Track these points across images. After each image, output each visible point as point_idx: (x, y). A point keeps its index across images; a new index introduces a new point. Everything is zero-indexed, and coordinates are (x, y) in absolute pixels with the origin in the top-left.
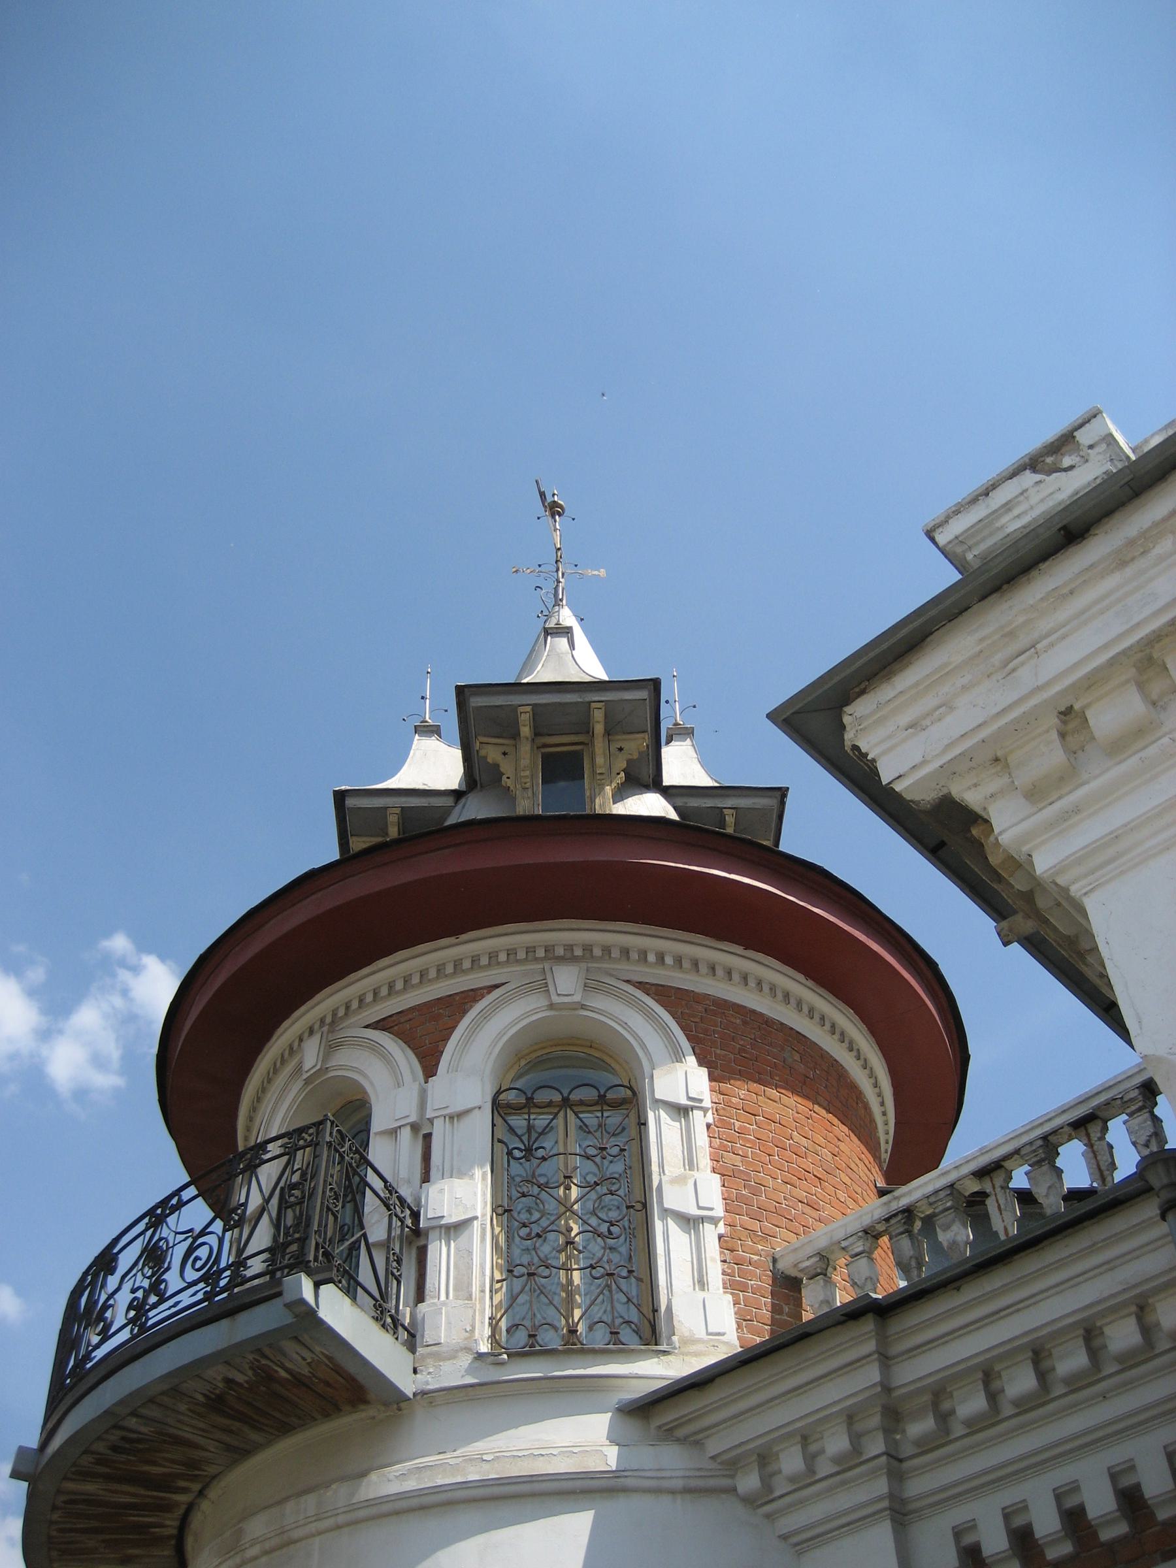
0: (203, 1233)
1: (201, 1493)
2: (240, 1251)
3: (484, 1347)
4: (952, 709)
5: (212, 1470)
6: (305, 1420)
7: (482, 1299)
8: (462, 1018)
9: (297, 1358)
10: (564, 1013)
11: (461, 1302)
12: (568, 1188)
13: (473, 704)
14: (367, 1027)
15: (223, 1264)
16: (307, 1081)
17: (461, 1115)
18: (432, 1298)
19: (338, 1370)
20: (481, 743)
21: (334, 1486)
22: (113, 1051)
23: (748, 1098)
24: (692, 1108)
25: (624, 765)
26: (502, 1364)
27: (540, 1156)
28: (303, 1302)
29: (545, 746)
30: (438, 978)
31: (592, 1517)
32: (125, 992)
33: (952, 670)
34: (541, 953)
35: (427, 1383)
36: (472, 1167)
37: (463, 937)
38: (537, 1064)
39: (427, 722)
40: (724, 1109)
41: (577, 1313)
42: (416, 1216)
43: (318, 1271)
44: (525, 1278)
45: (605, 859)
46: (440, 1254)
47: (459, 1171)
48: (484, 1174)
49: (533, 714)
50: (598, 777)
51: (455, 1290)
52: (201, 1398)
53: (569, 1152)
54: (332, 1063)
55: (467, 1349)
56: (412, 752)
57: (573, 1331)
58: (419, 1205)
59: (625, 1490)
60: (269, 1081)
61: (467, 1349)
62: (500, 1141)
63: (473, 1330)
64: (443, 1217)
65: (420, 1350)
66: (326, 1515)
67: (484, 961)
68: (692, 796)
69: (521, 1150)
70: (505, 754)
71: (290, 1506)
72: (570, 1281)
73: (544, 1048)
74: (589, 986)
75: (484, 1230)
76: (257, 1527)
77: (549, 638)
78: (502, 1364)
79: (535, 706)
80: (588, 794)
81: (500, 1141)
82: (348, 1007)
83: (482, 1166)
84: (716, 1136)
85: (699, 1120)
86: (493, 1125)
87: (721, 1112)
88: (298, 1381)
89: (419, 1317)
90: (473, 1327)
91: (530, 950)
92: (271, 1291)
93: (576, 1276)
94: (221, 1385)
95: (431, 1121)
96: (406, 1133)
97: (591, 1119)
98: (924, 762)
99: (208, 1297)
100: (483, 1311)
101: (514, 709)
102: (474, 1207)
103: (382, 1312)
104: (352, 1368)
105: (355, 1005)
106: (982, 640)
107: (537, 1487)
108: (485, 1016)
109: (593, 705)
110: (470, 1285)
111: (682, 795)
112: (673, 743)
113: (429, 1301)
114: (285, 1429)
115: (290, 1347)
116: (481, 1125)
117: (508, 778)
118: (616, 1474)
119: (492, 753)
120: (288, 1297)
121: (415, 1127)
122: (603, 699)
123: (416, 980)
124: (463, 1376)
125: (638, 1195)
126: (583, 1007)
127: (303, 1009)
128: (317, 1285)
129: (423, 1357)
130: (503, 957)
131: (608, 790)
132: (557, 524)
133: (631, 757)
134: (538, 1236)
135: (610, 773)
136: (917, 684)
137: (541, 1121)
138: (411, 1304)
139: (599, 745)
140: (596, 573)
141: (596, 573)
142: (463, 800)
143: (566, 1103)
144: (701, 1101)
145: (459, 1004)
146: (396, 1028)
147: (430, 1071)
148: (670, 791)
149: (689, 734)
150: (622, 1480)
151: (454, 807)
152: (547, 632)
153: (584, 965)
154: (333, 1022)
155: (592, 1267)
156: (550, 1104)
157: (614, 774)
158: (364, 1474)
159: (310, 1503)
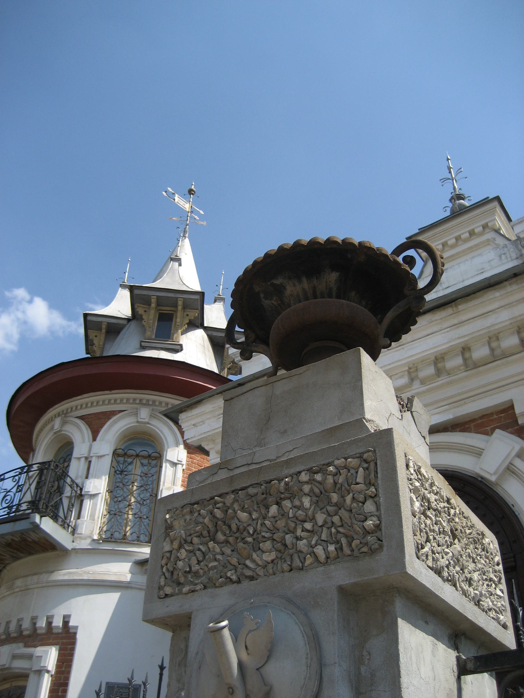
0: (9, 491)
1: (4, 567)
2: (20, 500)
3: (96, 537)
4: (204, 423)
5: (7, 562)
6: (37, 552)
7: (98, 521)
8: (108, 420)
9: (34, 536)
10: (142, 425)
11: (91, 521)
12: (133, 486)
13: (135, 293)
14: (77, 417)
15: (14, 504)
16: (55, 433)
17: (101, 456)
18: (82, 518)
19: (47, 540)
20: (137, 306)
21: (43, 574)
22: (16, 336)
23: (200, 460)
24: (178, 464)
25: (188, 321)
26: (100, 543)
27: (125, 474)
28: (35, 523)
29: (160, 310)
30: (102, 405)
32: (24, 312)
33: (205, 413)
34: (138, 401)
35: (76, 546)
36: (102, 475)
37: (113, 392)
38: (130, 440)
39: (125, 282)
40: (190, 464)
41: (128, 528)
42: (81, 489)
43: (43, 512)
44: (113, 515)
45: (161, 374)
46: (88, 504)
47: (98, 477)
48: (106, 478)
49: (157, 299)
50: (177, 326)
51: (90, 516)
52: (3, 543)
53: (136, 474)
54: (64, 429)
55: (90, 537)
56: (117, 295)
57: (125, 535)
58: (83, 486)
59: (131, 588)
60: (44, 427)
62: (113, 467)
63: (93, 531)
64: (89, 492)
65: (76, 535)
66: (40, 583)
67: (118, 401)
68: (214, 331)
69: (120, 471)
70: (145, 311)
71: (29, 578)
72: (128, 518)
73: (135, 434)
74: (152, 416)
76: (19, 583)
77: (172, 262)
78: (100, 543)
79: (157, 296)
80: (172, 331)
81: (113, 467)
82: (72, 409)
83: (105, 475)
84: (186, 473)
85: (180, 468)
86: (112, 461)
87: (189, 465)
88: (34, 542)
89: (77, 524)
90: (93, 529)
91: (135, 400)
92: (25, 517)
93: (130, 517)
94: (10, 541)
95: (92, 457)
96: (83, 460)
97: (145, 461)
98: (194, 437)
99: (9, 513)
100: (97, 525)
101: (150, 296)
102: (100, 490)
103: (64, 523)
104: (52, 541)
105: (74, 409)
106: (213, 408)
107: (104, 583)
108: (115, 422)
109: (179, 299)
110: (95, 515)
111: (212, 330)
112: (216, 303)
113: (81, 519)
114: (30, 554)
115: (31, 533)
116: (107, 462)
117: (145, 322)
118: (129, 583)
119: (140, 311)
120: (31, 520)
121: (86, 458)
122: (183, 297)
123: (95, 404)
124: (88, 546)
125: (155, 492)
126: (148, 423)
127: (57, 406)
128: (41, 517)
129: (76, 537)
130: (125, 401)
131: (180, 331)
132: (191, 199)
133: (190, 318)
134: (120, 501)
135: (181, 326)
136: (197, 414)
137: (130, 460)
138: (76, 519)
139: (179, 314)
140: (202, 223)
141: (202, 223)
142: (130, 322)
143: (137, 456)
144: (181, 462)
145: (107, 416)
146: (86, 420)
147: (94, 439)
148: (207, 328)
149: (223, 300)
150: (130, 584)
151: (126, 325)
152: (172, 259)
153: (151, 408)
154: (65, 414)
155: (135, 514)
156: (132, 455)
157: (183, 325)
158: (53, 572)
159: (35, 578)
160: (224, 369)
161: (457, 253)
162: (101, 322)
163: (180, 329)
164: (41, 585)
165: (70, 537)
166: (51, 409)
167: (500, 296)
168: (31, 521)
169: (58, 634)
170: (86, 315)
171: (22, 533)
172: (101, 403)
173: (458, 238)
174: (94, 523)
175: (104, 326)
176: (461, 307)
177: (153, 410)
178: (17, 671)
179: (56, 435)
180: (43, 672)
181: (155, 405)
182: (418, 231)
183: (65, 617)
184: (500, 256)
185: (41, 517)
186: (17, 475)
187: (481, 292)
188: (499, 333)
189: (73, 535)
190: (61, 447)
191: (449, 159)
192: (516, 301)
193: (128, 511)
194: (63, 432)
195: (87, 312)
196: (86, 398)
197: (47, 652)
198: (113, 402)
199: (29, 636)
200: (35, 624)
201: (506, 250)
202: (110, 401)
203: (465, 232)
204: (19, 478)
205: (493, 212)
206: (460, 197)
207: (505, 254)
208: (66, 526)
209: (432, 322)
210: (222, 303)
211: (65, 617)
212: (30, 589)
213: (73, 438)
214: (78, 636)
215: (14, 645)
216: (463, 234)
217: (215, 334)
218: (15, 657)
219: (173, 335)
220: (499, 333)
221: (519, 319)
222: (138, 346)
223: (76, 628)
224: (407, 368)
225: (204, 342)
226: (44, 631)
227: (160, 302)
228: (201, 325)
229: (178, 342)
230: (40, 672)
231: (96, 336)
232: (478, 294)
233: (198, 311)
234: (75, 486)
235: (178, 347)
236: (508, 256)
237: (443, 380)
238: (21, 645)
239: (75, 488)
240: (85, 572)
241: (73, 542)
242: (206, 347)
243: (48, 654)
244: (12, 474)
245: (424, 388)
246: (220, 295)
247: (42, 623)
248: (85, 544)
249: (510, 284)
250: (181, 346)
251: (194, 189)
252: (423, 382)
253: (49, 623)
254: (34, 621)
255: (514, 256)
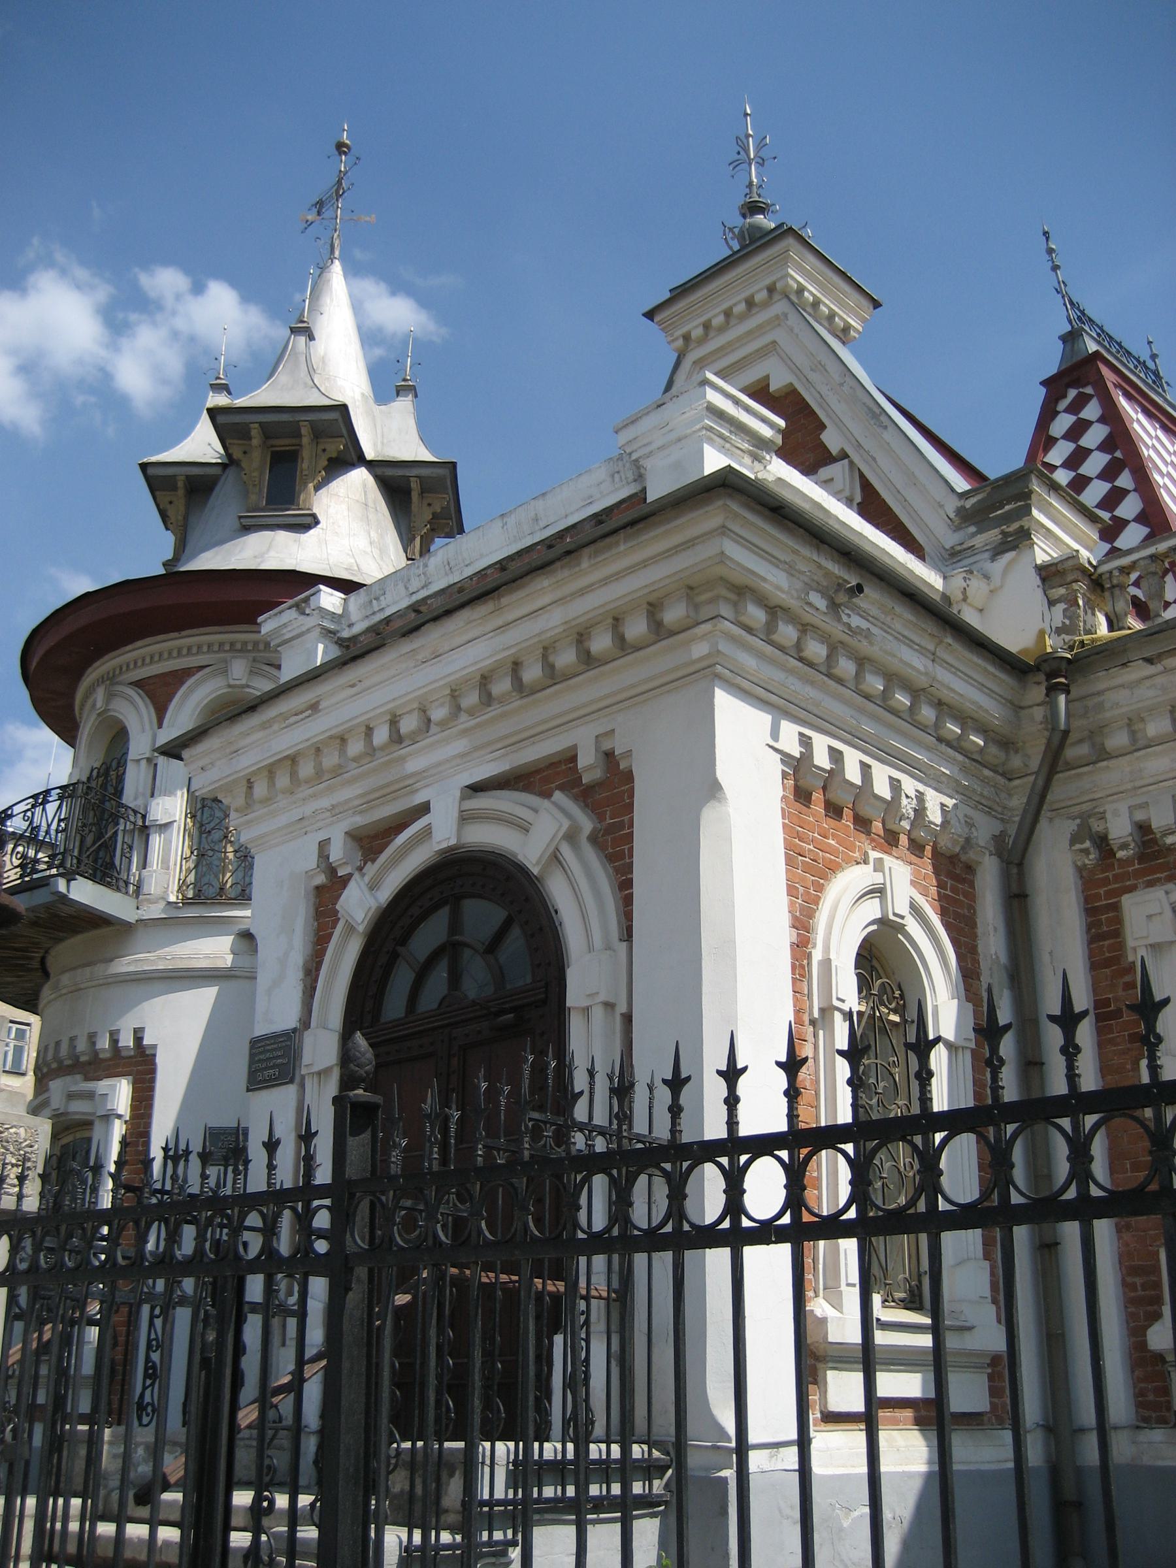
14: (131, 684)
16: (99, 715)
26: (179, 908)
29: (272, 446)
31: (1104, 492)
34: (227, 647)
36: (176, 789)
37: (184, 633)
39: (220, 378)
42: (144, 817)
47: (170, 793)
55: (163, 898)
61: (163, 898)
67: (194, 650)
74: (252, 673)
75: (179, 828)
76: (65, 979)
78: (179, 908)
79: (260, 423)
83: (182, 789)
91: (221, 644)
93: (231, 856)
96: (144, 763)
98: (203, 787)
99: (22, 877)
104: (99, 913)
108: (191, 691)
113: (148, 869)
119: (237, 454)
126: (248, 686)
128: (69, 881)
131: (311, 486)
139: (306, 453)
142: (227, 471)
145: (178, 678)
154: (110, 679)
158: (111, 960)
159: (88, 969)
160: (414, 538)
161: (728, 343)
162: (174, 477)
163: (313, 482)
164: (96, 982)
165: (130, 902)
166: (90, 670)
167: (550, 585)
168: (53, 890)
169: (131, 1057)
170: (144, 467)
171: (47, 907)
172: (166, 655)
173: (728, 314)
174: (169, 874)
175: (180, 484)
176: (504, 601)
177: (254, 660)
178: (77, 1117)
179: (101, 719)
180: (112, 1117)
181: (259, 651)
182: (668, 295)
183: (136, 1031)
184: (613, 476)
185: (69, 881)
186: (28, 810)
187: (529, 577)
188: (555, 642)
189: (137, 897)
190: (113, 738)
191: (747, 114)
192: (572, 595)
193: (225, 847)
194: (112, 713)
195: (145, 460)
196: (141, 648)
197: (113, 1087)
198: (185, 651)
199: (89, 1063)
200: (94, 1044)
201: (620, 463)
202: (180, 650)
203: (739, 302)
204: (33, 814)
205: (783, 258)
206: (754, 208)
207: (618, 472)
208: (122, 884)
209: (471, 622)
210: (410, 397)
211: (136, 1031)
212: (81, 989)
213: (125, 721)
214: (158, 1060)
215: (68, 1079)
216: (735, 305)
217: (390, 472)
218: (71, 1096)
219: (299, 497)
220: (555, 642)
221: (574, 623)
222: (237, 525)
223: (154, 1047)
224: (448, 692)
225: (365, 495)
226: (108, 1055)
227: (268, 432)
228: (360, 459)
229: (309, 509)
230: (109, 1117)
231: (171, 503)
232: (525, 579)
233: (343, 440)
234: (131, 812)
235: (309, 520)
236: (623, 477)
237: (494, 711)
238: (78, 1077)
239: (132, 819)
240: (160, 958)
241: (138, 908)
242: (371, 504)
243: (115, 1090)
244: (22, 807)
245: (473, 723)
246: (407, 380)
247: (104, 1043)
248: (155, 911)
249: (562, 567)
250: (314, 516)
251: (348, 142)
252: (471, 712)
253: (114, 1041)
254: (92, 1038)
255: (631, 476)
